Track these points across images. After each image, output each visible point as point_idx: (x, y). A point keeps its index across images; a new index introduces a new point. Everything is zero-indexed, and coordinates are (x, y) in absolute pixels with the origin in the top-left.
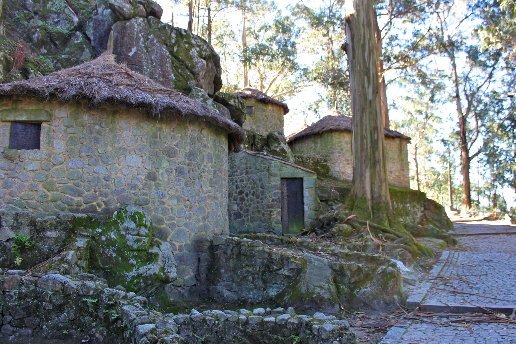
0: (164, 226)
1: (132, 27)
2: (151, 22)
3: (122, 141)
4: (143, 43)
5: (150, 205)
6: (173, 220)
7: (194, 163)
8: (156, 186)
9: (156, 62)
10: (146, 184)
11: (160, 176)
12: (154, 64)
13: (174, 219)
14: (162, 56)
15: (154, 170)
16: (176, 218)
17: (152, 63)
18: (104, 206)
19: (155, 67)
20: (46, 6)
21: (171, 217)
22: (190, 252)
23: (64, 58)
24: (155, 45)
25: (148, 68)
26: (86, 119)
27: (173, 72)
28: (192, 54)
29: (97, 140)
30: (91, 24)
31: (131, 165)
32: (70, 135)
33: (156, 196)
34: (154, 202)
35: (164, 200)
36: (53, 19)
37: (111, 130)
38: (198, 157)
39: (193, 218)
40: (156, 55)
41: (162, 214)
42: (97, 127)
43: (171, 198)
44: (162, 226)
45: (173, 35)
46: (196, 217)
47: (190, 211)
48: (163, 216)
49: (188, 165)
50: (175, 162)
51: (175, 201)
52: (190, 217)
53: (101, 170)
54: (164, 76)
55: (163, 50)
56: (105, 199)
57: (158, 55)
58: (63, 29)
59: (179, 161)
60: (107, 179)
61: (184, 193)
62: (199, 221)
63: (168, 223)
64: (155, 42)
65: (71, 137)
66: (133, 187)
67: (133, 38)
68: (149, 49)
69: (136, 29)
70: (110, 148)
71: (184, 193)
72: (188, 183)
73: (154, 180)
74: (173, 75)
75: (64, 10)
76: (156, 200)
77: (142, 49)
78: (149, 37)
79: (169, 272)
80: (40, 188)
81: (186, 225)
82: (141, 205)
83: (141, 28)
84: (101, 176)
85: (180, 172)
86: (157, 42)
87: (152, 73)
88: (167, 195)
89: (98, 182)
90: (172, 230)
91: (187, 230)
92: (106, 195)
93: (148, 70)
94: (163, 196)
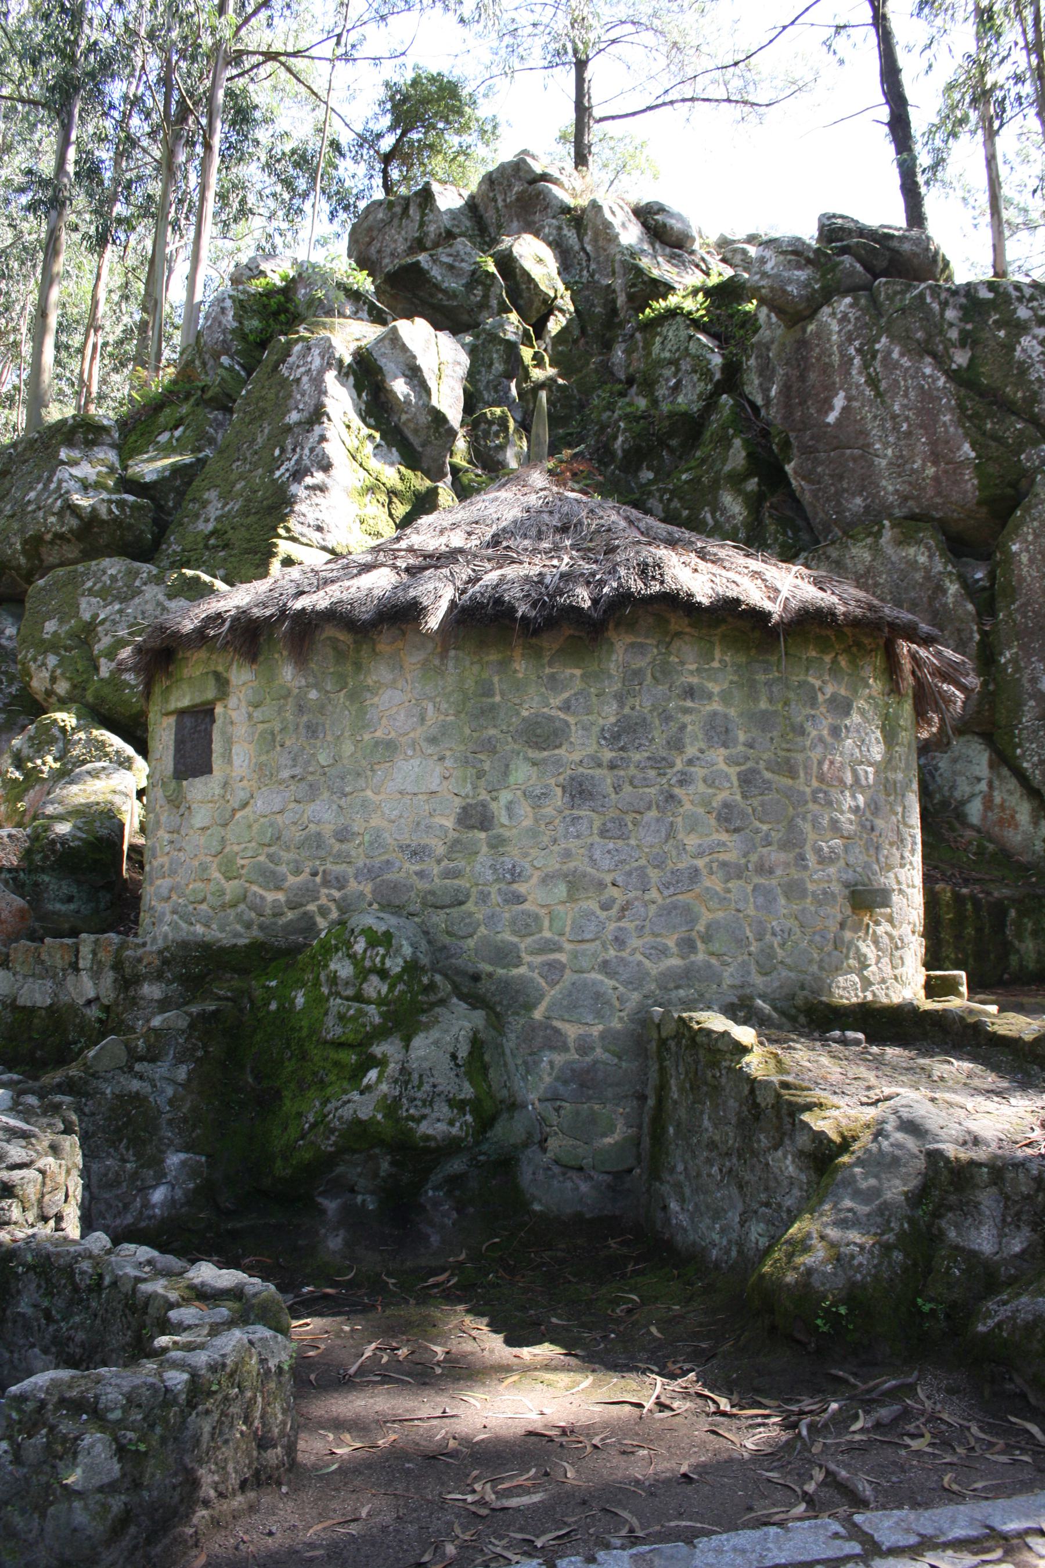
0: (522, 970)
1: (822, 333)
2: (882, 297)
3: (384, 721)
4: (860, 373)
5: (470, 906)
6: (553, 951)
7: (637, 757)
8: (492, 846)
9: (907, 419)
10: (457, 841)
11: (504, 812)
12: (905, 426)
13: (560, 949)
14: (927, 395)
15: (484, 796)
16: (568, 946)
17: (896, 429)
18: (334, 915)
19: (909, 434)
20: (650, 354)
21: (548, 941)
22: (620, 1058)
23: (686, 482)
24: (896, 365)
25: (886, 445)
26: (289, 677)
27: (966, 435)
28: (1023, 357)
29: (312, 730)
30: (752, 362)
31: (410, 789)
32: (261, 727)
33: (490, 878)
34: (484, 897)
35: (521, 888)
36: (668, 380)
37: (354, 696)
38: (656, 734)
39: (634, 942)
40: (906, 395)
41: (514, 933)
42: (313, 694)
43: (546, 880)
44: (515, 972)
45: (951, 314)
46: (648, 939)
47: (619, 919)
48: (515, 939)
49: (612, 766)
50: (558, 762)
51: (561, 890)
52: (619, 942)
53: (323, 814)
54: (935, 458)
55: (924, 377)
56: (337, 894)
57: (912, 394)
58: (688, 400)
59: (576, 757)
60: (343, 835)
61: (593, 860)
62: (664, 952)
63: (539, 959)
64: (895, 355)
65: (265, 731)
66: (417, 853)
67: (830, 365)
68: (883, 385)
69: (835, 337)
70: (348, 748)
71: (593, 860)
72: (609, 825)
73: (483, 828)
74: (966, 447)
75: (687, 349)
76: (493, 890)
77: (862, 393)
78: (877, 346)
79: (412, 1118)
80: (217, 875)
81: (605, 967)
82: (442, 907)
83: (850, 327)
84: (327, 830)
85: (579, 791)
86: (902, 355)
87: (902, 456)
88: (530, 870)
89: (318, 847)
90: (553, 984)
91: (612, 983)
92: (341, 883)
93: (889, 452)
94: (516, 875)
